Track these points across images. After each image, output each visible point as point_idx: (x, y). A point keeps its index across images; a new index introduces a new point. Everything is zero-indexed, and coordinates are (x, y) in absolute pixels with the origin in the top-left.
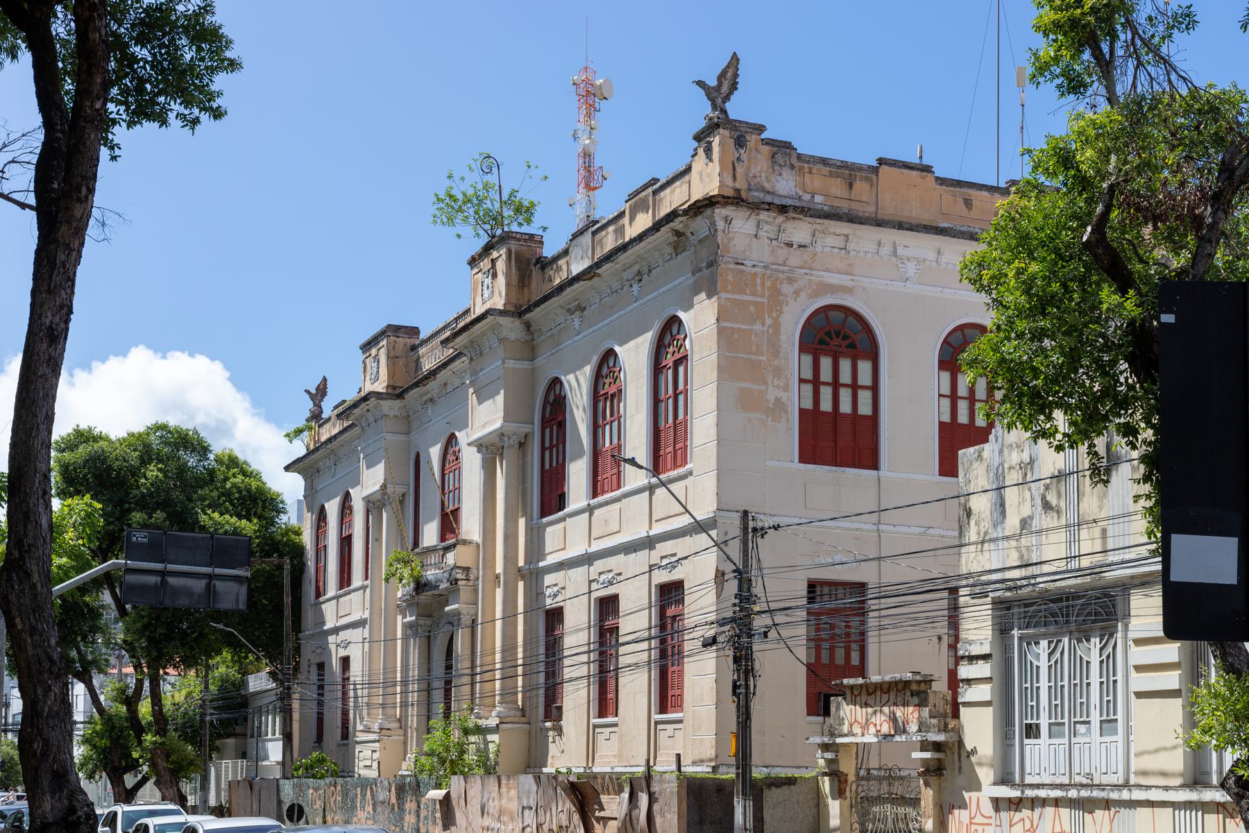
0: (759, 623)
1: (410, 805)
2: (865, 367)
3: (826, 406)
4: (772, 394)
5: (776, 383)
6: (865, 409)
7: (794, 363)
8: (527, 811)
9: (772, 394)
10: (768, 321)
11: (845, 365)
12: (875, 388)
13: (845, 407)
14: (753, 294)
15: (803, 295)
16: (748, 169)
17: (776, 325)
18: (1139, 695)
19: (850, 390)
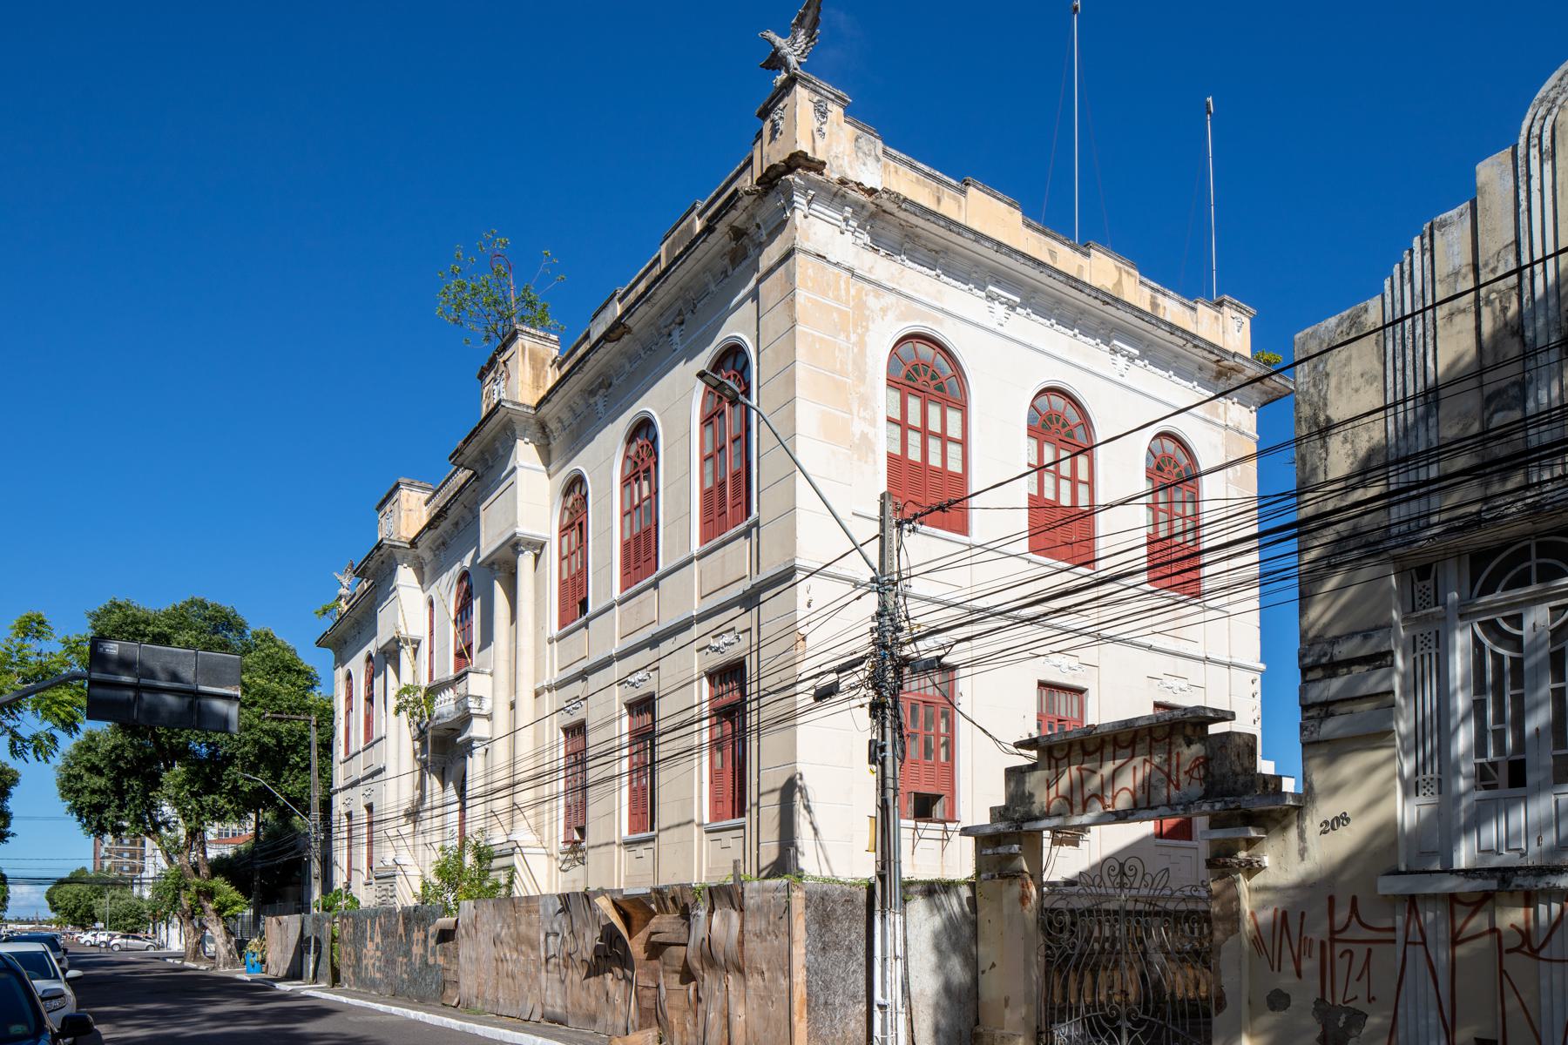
0: (1142, 920)
1: (417, 935)
2: (954, 417)
3: (915, 455)
4: (858, 427)
5: (862, 414)
6: (955, 466)
7: (884, 401)
8: (551, 938)
9: (858, 427)
10: (854, 338)
11: (934, 412)
12: (964, 443)
13: (935, 460)
14: (837, 298)
15: (891, 315)
16: (830, 145)
17: (862, 344)
18: (1369, 951)
19: (910, 422)
